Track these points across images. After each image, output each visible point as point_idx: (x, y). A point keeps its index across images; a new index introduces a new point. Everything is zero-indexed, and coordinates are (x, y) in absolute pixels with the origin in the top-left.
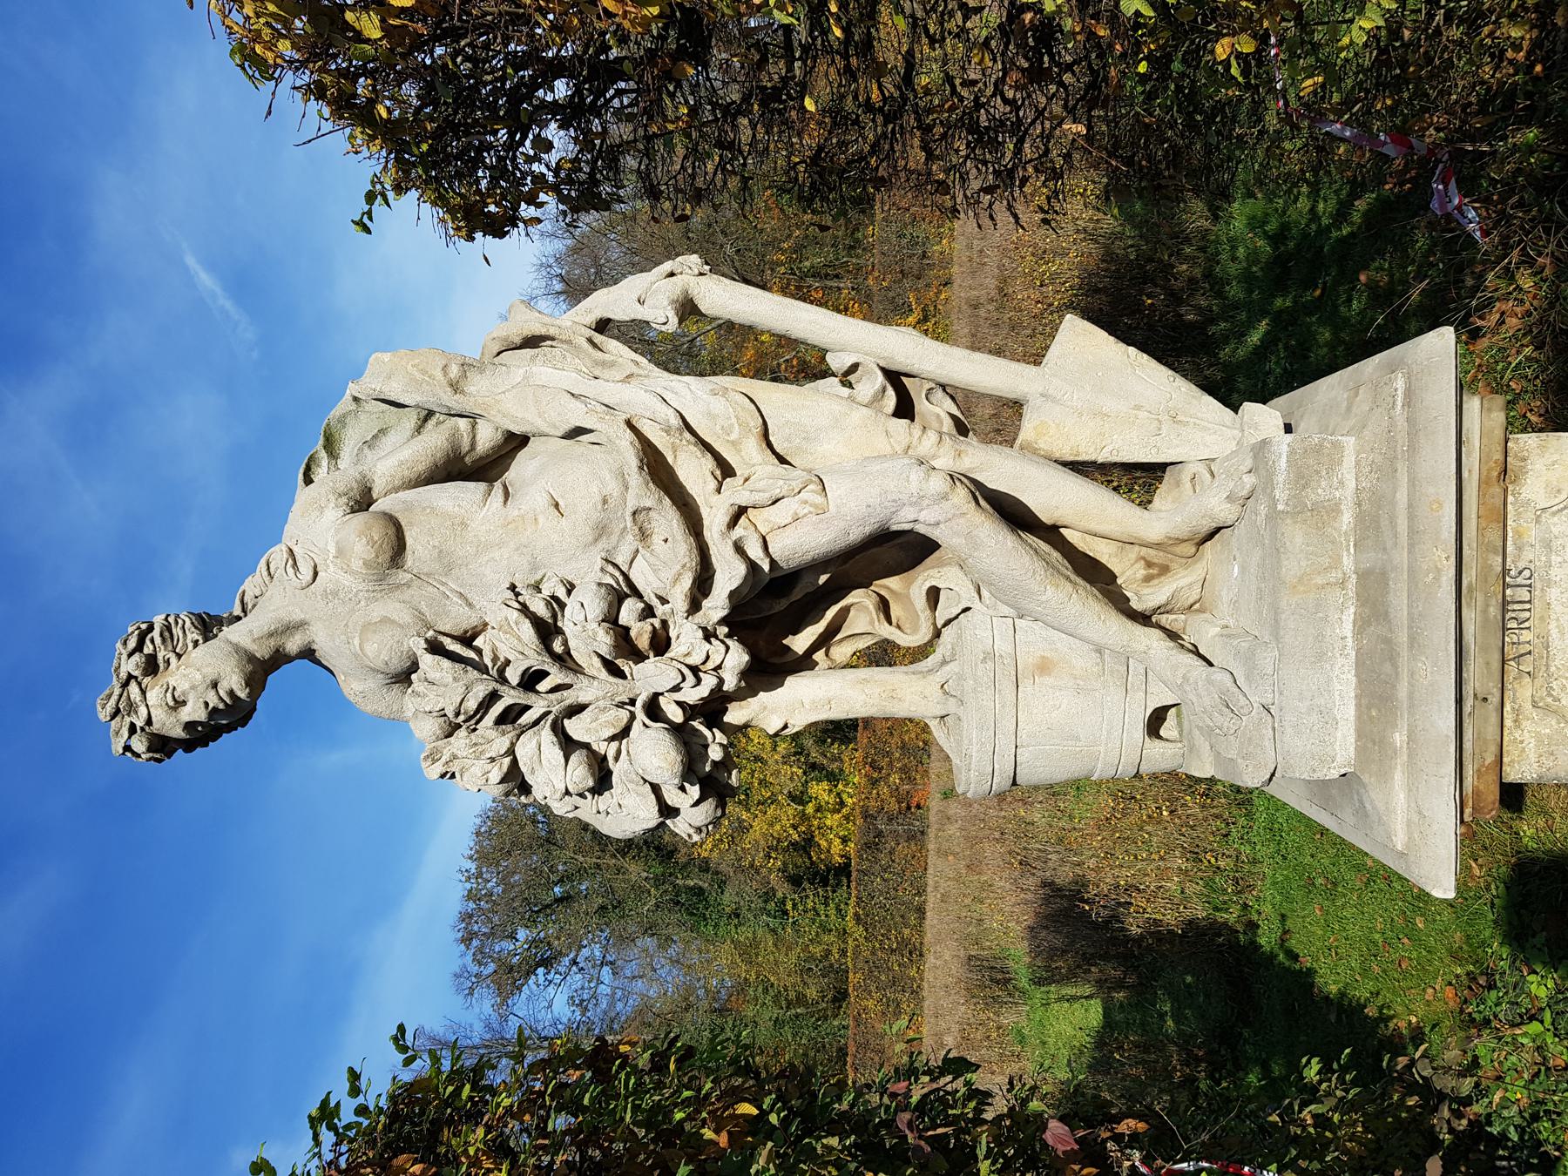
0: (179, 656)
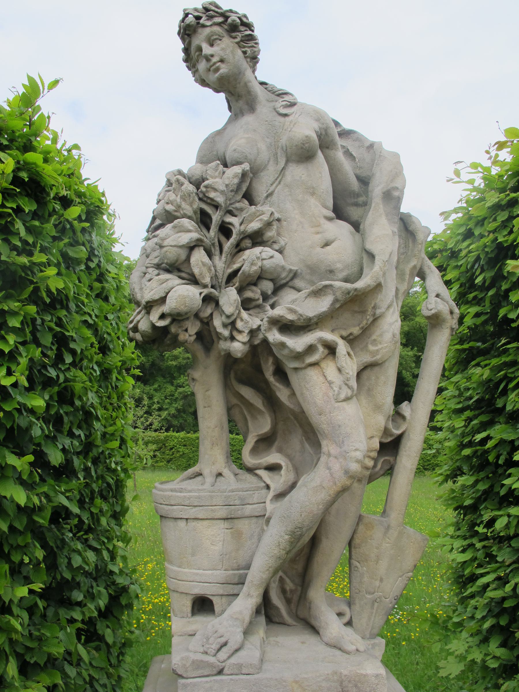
0: (237, 43)
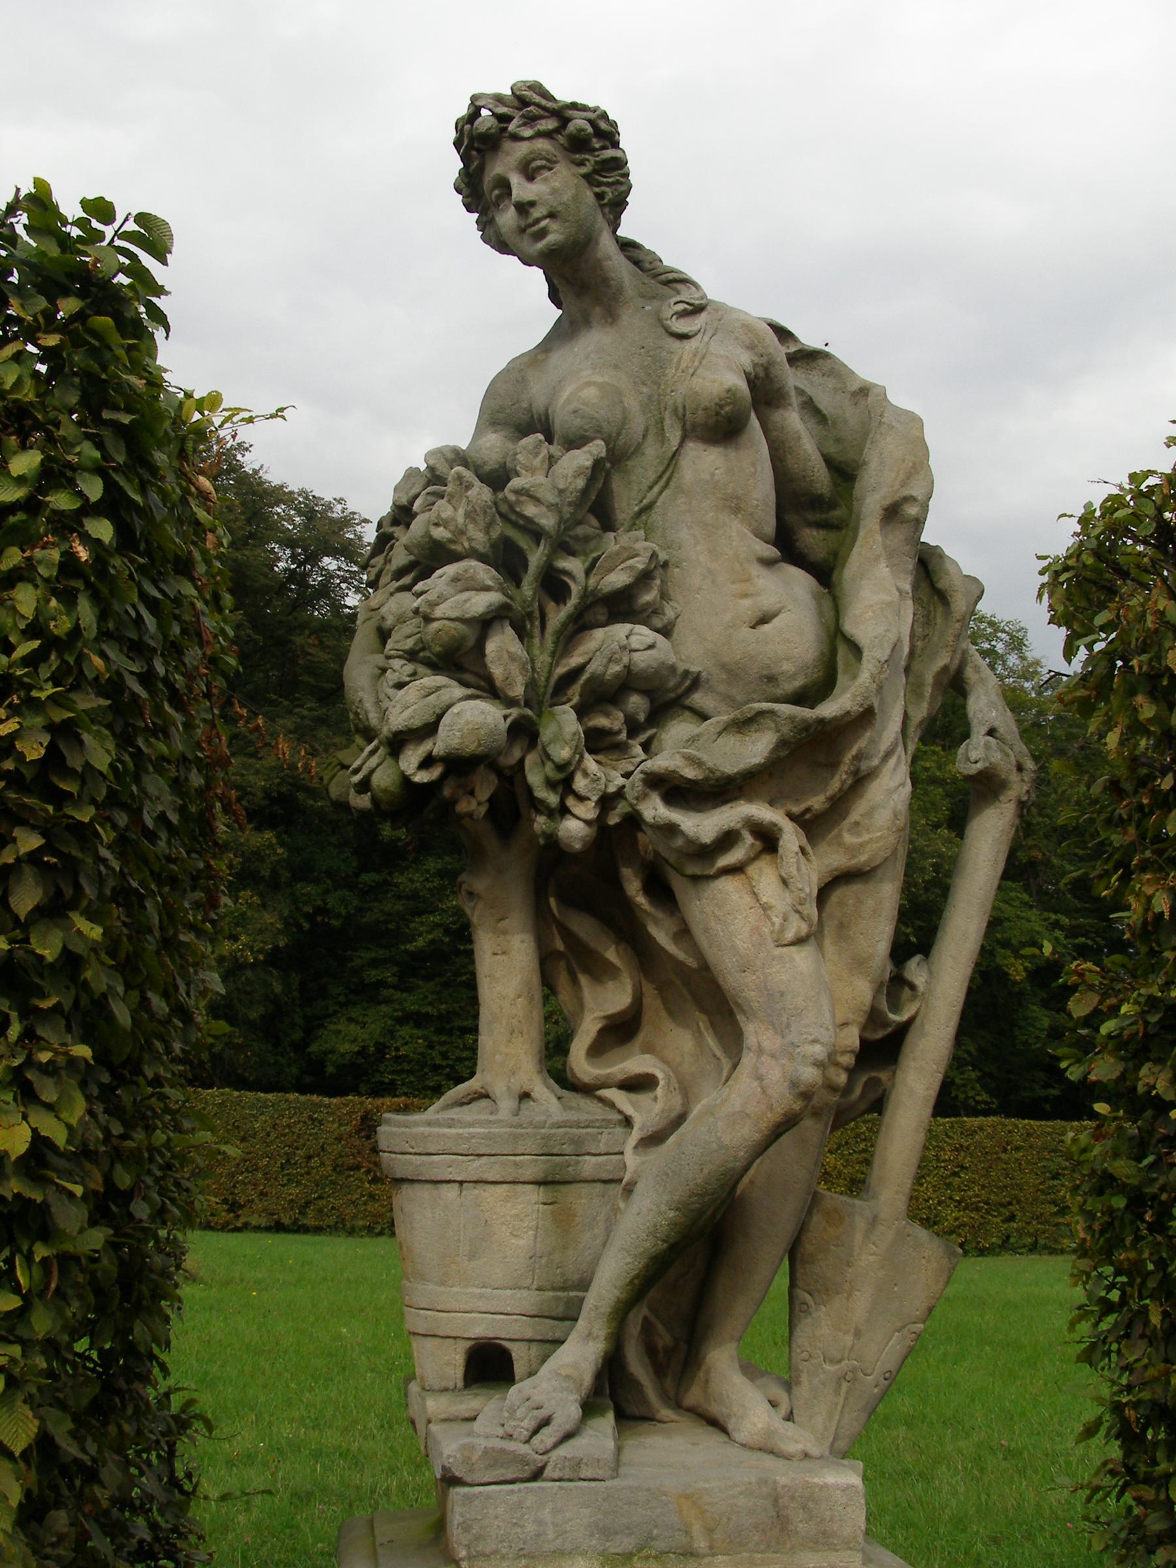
0: (585, 176)
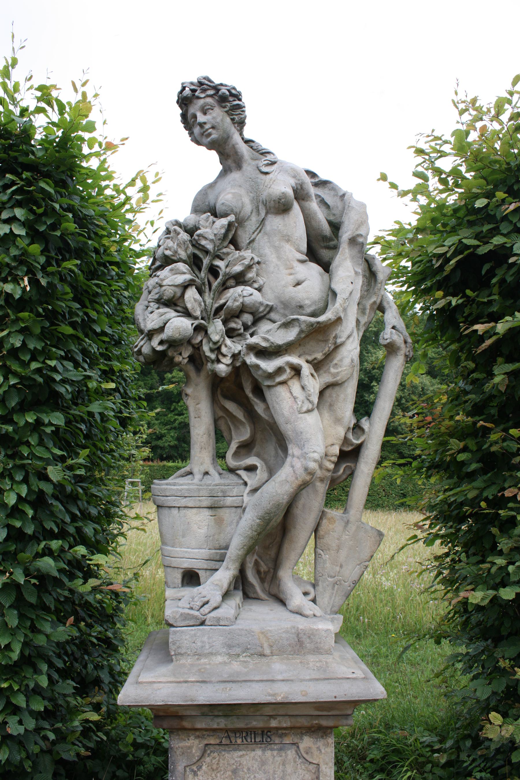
0: (226, 112)
